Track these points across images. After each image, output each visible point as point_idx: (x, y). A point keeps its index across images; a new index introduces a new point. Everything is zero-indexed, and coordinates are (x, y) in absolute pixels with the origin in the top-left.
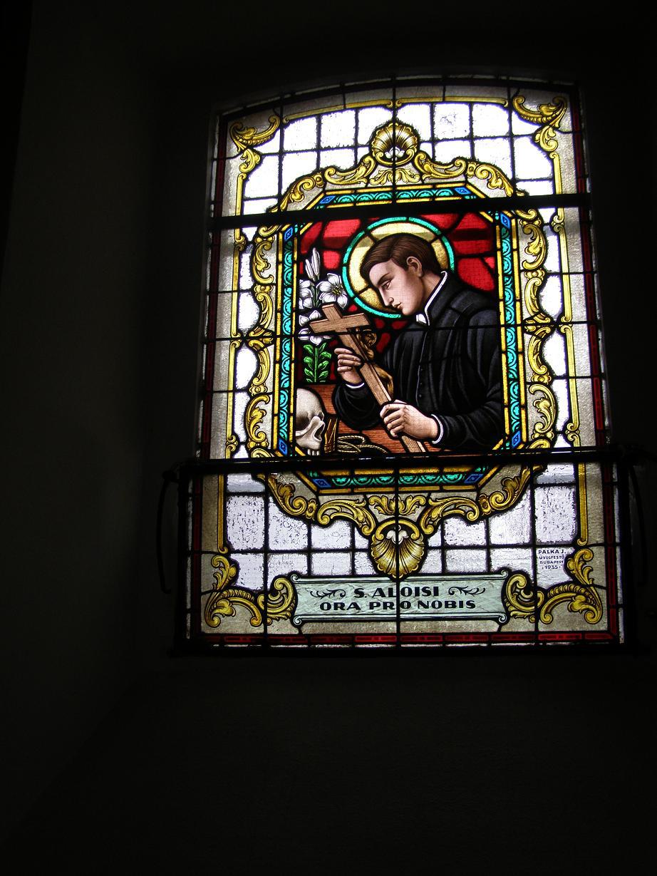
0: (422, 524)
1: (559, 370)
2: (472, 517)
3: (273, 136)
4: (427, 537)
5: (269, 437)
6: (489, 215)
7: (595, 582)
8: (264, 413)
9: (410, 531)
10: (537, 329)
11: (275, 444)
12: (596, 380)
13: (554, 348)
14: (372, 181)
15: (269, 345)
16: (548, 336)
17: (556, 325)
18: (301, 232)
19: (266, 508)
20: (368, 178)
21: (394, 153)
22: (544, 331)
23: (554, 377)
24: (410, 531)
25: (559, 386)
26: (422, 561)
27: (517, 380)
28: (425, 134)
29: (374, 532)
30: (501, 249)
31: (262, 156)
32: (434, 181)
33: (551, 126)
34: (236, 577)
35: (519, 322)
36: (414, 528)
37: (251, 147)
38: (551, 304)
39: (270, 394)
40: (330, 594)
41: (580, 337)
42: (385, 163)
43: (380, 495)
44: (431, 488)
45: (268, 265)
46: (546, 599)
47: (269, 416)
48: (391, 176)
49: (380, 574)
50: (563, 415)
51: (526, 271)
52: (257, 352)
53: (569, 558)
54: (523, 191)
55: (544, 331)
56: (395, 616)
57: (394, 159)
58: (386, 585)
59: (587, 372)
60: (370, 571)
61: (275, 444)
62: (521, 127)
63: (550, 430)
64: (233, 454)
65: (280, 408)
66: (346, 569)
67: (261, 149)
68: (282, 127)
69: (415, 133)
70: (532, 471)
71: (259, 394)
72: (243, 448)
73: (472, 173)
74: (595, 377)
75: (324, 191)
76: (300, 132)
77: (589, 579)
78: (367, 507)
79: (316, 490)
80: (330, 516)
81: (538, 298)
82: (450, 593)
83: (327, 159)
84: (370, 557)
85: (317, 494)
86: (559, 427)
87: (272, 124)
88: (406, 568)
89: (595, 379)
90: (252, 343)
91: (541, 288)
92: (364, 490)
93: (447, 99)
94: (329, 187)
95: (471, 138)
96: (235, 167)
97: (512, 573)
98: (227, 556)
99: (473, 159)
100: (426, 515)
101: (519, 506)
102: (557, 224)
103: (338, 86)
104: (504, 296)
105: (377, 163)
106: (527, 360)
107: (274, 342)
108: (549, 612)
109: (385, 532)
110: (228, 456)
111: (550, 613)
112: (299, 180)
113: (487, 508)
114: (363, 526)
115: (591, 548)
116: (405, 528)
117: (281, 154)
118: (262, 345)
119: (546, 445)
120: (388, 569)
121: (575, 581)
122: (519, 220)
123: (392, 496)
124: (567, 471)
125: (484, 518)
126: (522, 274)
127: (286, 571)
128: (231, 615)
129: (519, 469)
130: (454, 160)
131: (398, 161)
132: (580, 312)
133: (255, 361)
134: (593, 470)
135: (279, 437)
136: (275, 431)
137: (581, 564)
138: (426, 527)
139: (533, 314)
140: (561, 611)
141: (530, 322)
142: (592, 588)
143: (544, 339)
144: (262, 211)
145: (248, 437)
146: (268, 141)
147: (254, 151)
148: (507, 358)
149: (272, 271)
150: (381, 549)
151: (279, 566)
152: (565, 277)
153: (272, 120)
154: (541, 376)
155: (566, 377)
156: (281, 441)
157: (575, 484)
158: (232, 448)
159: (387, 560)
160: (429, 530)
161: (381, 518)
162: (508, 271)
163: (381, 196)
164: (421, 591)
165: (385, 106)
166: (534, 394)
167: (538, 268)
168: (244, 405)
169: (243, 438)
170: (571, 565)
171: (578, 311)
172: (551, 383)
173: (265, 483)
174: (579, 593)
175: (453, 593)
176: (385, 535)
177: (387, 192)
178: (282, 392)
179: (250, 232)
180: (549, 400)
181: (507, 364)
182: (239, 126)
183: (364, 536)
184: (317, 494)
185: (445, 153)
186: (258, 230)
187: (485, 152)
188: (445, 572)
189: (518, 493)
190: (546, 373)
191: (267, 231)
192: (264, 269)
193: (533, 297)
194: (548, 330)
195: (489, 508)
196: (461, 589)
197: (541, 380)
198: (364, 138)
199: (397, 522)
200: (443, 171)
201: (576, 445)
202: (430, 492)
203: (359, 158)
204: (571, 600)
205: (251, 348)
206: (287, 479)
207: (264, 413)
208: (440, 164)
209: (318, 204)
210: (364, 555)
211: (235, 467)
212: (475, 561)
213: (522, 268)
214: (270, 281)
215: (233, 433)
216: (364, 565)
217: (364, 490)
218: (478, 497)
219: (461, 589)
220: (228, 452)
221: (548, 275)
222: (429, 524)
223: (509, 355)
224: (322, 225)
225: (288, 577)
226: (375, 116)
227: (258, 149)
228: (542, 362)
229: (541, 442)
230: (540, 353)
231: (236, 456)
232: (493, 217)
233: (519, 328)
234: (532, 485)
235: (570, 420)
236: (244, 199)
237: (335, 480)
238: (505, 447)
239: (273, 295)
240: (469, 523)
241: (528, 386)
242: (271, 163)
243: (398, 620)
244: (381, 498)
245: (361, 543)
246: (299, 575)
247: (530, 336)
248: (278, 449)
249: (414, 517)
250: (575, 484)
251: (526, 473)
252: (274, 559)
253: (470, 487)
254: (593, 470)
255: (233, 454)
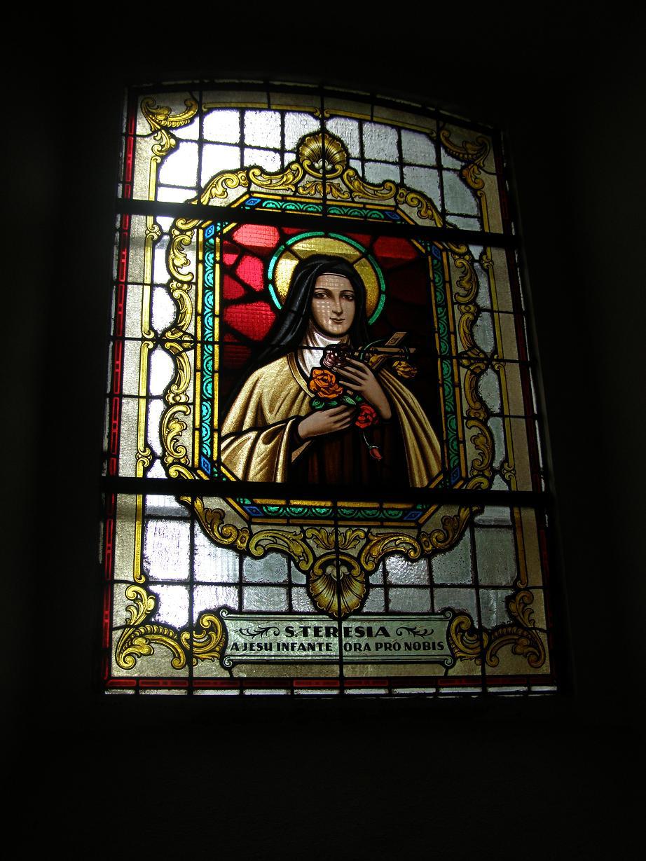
0: (362, 560)
1: (160, 293)
2: (257, 172)
3: (192, 120)
4: (297, 161)
5: (190, 450)
6: (420, 244)
7: (537, 625)
8: (459, 284)
9: (351, 568)
10: (181, 337)
11: (196, 460)
12: (122, 278)
13: (164, 316)
14: (362, 534)
15: (188, 349)
16: (483, 372)
17: (160, 341)
18: (225, 231)
19: (192, 536)
20: (369, 541)
21: (338, 572)
22: (173, 334)
23: (167, 286)
24: (311, 167)
25: (495, 424)
26: (363, 599)
27: (455, 413)
28: (354, 151)
29: (344, 171)
30: (434, 281)
31: (178, 141)
32: (365, 201)
33: (476, 164)
34: (155, 611)
35: (454, 354)
36: (354, 563)
37: (168, 129)
38: (162, 364)
39: (191, 404)
40: (263, 632)
41: (133, 327)
42: (346, 559)
43: (339, 199)
44: (293, 199)
45: (187, 263)
46: (490, 642)
47: (454, 283)
48: (320, 187)
49: (320, 612)
50: (499, 457)
51: (186, 404)
52: (175, 356)
53: (509, 600)
54: (451, 225)
55: (173, 334)
56: (338, 658)
57: (337, 563)
58: (324, 623)
59: (522, 413)
60: (310, 608)
61: (196, 460)
62: (447, 161)
63: (488, 468)
64: (146, 470)
65: (201, 421)
66: (283, 607)
67: (178, 133)
68: (202, 115)
69: (344, 148)
70: (471, 510)
71: (466, 304)
72: (158, 462)
73: (402, 200)
74: (123, 283)
75: (249, 192)
76: (221, 123)
77: (530, 621)
78: (304, 540)
79: (248, 519)
80: (264, 548)
81: (178, 369)
82: (398, 635)
83: (252, 158)
84: (309, 594)
85: (249, 522)
86: (496, 465)
87: (189, 109)
88: (347, 607)
89: (124, 281)
90: (168, 345)
91: (473, 322)
92: (301, 521)
93: (375, 119)
94: (253, 188)
95: (401, 163)
96: (146, 149)
97: (456, 613)
98: (145, 586)
99: (402, 185)
100: (297, 179)
101: (461, 542)
102: (146, 457)
103: (262, 82)
104: (439, 328)
105: (305, 172)
106: (463, 393)
107: (194, 348)
108: (493, 655)
109: (323, 567)
110: (140, 474)
111: (495, 655)
112: (451, 548)
113: (428, 546)
114: (300, 561)
115: (531, 590)
116: (317, 171)
117: (201, 142)
118: (181, 349)
119: (180, 223)
120: (329, 606)
121: (516, 623)
122: (190, 465)
123: (329, 529)
124: (503, 513)
125: (246, 170)
126: (191, 401)
127: (212, 605)
128: (150, 654)
129: (457, 509)
130: (385, 182)
131: (333, 560)
132: (511, 351)
133: (172, 365)
134: (529, 515)
135: (201, 453)
136: (197, 445)
137: (522, 607)
138: (298, 169)
139: (183, 354)
140: (504, 652)
141: (186, 345)
142: (534, 631)
143: (175, 326)
144: (182, 201)
145: (164, 450)
146: (185, 125)
147: (168, 133)
148: (444, 390)
149: (192, 268)
150: (320, 586)
151: (207, 599)
152: (143, 393)
153: (188, 103)
154: (179, 288)
155: (153, 286)
156: (203, 459)
157: (514, 526)
158: (144, 462)
159: (327, 596)
160: (370, 567)
161: (319, 552)
162: (208, 404)
163: (310, 207)
164: (366, 632)
165: (312, 114)
166: (470, 429)
167: (173, 405)
168: (159, 414)
169: (159, 451)
170: (513, 607)
171: (511, 350)
172: (170, 281)
173: (445, 222)
174: (522, 636)
175: (401, 633)
176: (333, 167)
177: (317, 204)
178: (210, 397)
179: (166, 222)
180: (174, 265)
181: (444, 397)
182: (150, 102)
183: (303, 572)
184: (249, 522)
185: (374, 174)
186: (175, 222)
187: (414, 178)
188: (387, 612)
189: (213, 184)
190: (173, 291)
191: (186, 224)
192: (477, 436)
193: (467, 331)
194: (483, 366)
195: (431, 546)
196: (409, 630)
197: (179, 284)
198: (290, 144)
199: (338, 556)
200: (279, 541)
201: (150, 219)
202: (294, 196)
203: (286, 164)
204: (516, 643)
205: (167, 351)
206: (214, 503)
207: (459, 284)
208: (369, 184)
209: (424, 511)
210: (303, 590)
211: (145, 486)
212: (419, 601)
213: (192, 407)
214: (472, 423)
215: (147, 445)
216: (301, 602)
217: (301, 521)
218: (418, 536)
219: (409, 630)
220: (489, 253)
221: (480, 310)
222: (296, 171)
223: (446, 388)
224: (482, 588)
225: (216, 612)
226: (301, 125)
227: (175, 133)
228: (178, 303)
229: (184, 227)
230: (475, 389)
231: (150, 475)
232: (425, 247)
233: (199, 339)
234: (471, 525)
235: (506, 460)
236: (158, 185)
237: (267, 509)
238: (221, 227)
239: (192, 294)
240: (413, 561)
241: (465, 421)
242: (188, 152)
243: (341, 663)
244: (338, 196)
245: (355, 164)
246: (230, 611)
247: (187, 331)
248: (442, 251)
249: (354, 553)
250: (514, 526)
251: (464, 513)
252: (200, 592)
253: (255, 195)
254: (529, 515)
255: (146, 470)
